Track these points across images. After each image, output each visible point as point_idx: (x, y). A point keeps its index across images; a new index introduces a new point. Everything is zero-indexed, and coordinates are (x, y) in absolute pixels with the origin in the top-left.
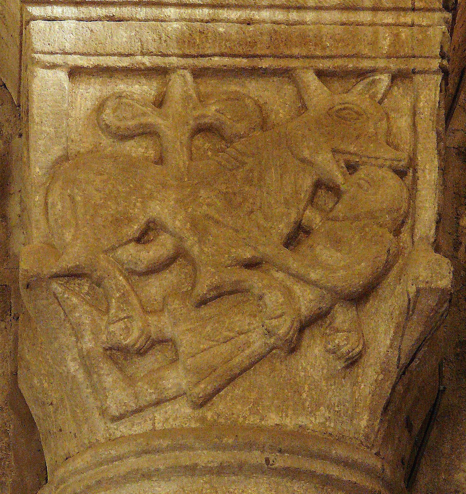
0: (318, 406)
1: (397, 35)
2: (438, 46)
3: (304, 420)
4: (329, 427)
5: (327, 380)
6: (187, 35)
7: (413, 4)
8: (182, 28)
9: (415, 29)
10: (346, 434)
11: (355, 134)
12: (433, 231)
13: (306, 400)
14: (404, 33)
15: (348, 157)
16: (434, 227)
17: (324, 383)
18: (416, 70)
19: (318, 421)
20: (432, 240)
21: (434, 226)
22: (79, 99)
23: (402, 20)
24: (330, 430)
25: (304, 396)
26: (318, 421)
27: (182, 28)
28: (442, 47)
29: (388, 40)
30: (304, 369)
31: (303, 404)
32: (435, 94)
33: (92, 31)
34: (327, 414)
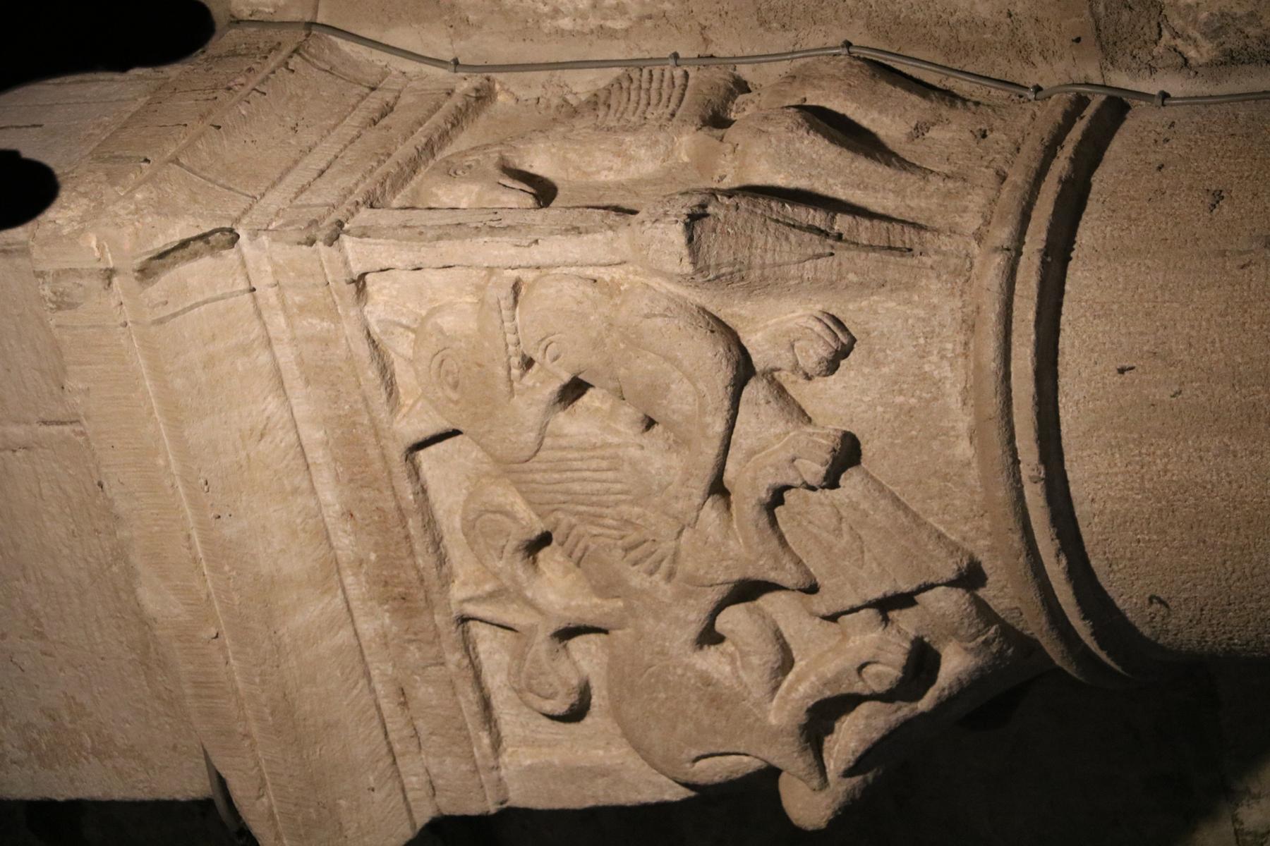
0: (924, 377)
1: (302, 308)
2: (297, 248)
3: (953, 400)
4: (954, 350)
5: (878, 364)
6: (396, 604)
7: (243, 292)
8: (387, 611)
9: (283, 281)
10: (959, 315)
11: (476, 369)
12: (599, 237)
13: (920, 398)
14: (295, 298)
15: (516, 372)
16: (590, 236)
17: (885, 370)
18: (460, 61)
19: (949, 375)
20: (610, 233)
21: (585, 238)
22: (543, 736)
23: (273, 300)
24: (959, 349)
25: (913, 401)
26: (949, 375)
27: (387, 611)
28: (299, 243)
29: (314, 322)
30: (872, 406)
31: (928, 402)
32: (376, 244)
33: (431, 734)
34: (934, 358)
